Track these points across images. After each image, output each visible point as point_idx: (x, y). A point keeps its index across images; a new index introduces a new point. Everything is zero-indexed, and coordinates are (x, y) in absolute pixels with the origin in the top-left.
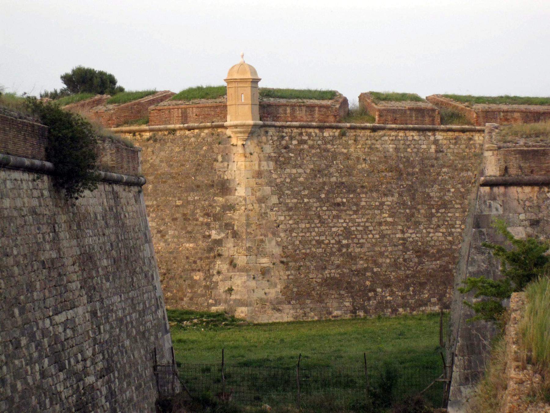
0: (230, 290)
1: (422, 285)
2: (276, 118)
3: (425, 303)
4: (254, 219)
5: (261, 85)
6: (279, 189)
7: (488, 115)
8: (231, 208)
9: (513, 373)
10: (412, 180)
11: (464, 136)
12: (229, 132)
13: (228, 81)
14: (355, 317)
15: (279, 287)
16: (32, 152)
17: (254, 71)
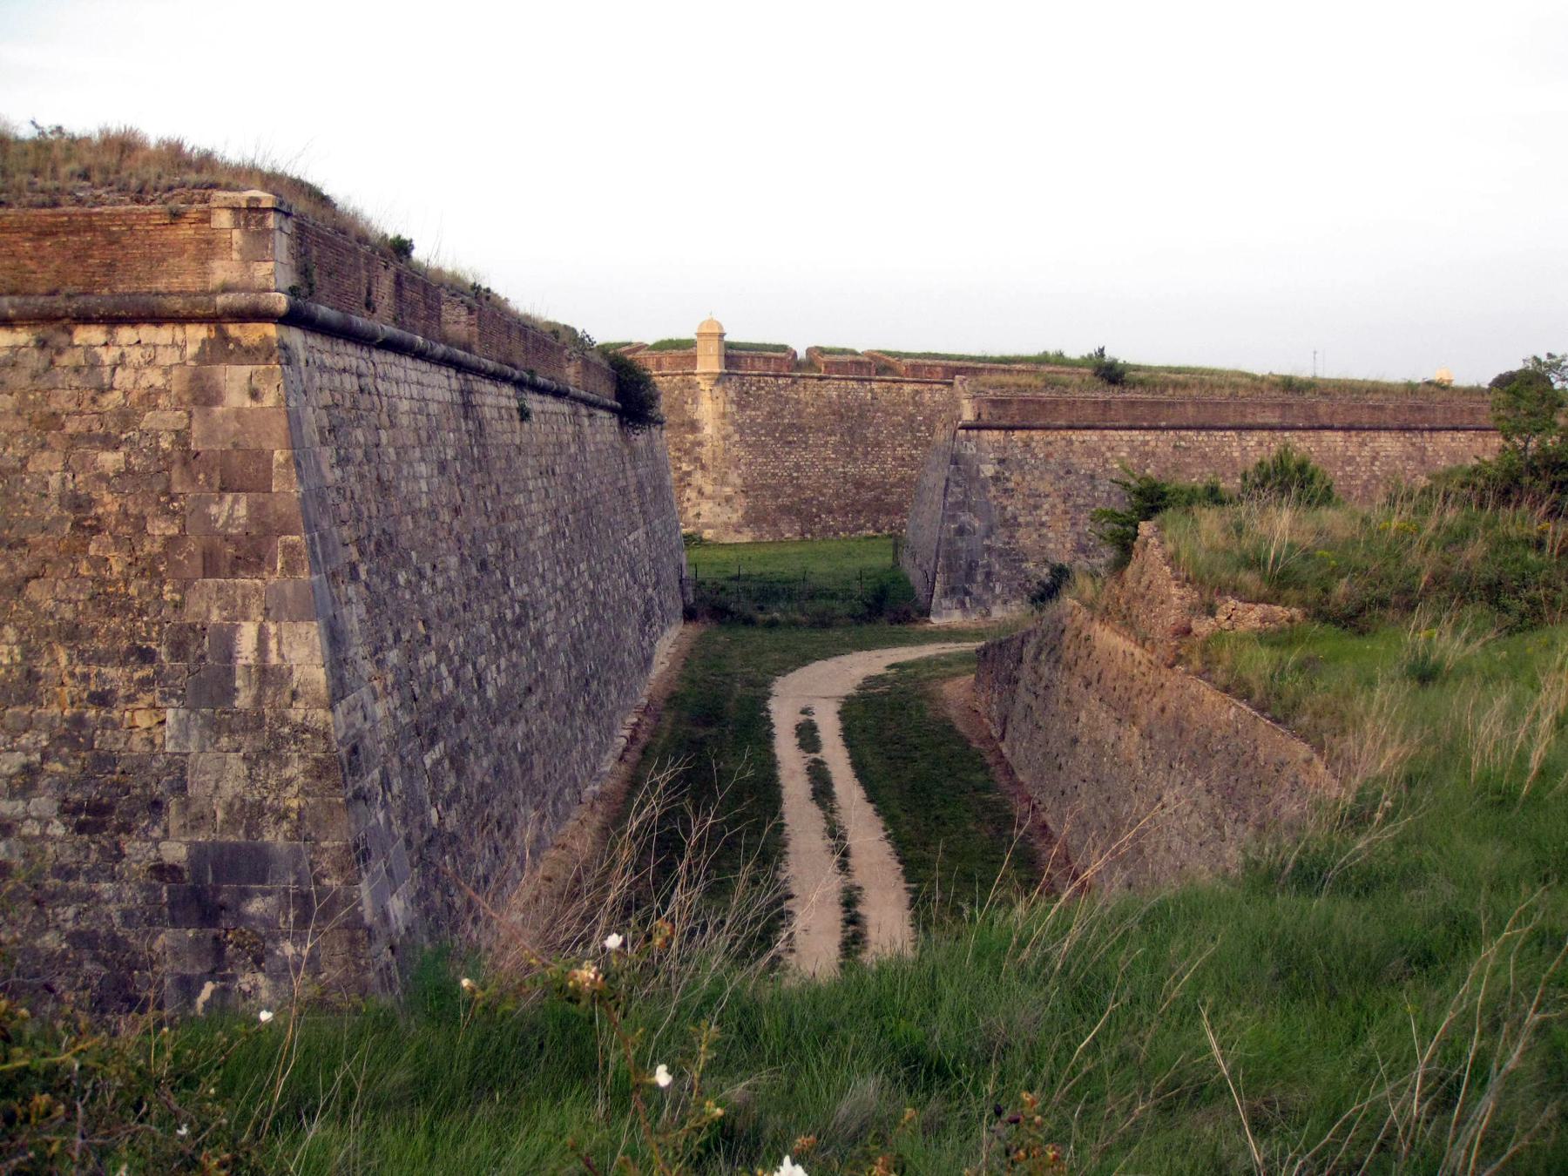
0: (698, 515)
1: (859, 512)
2: (738, 367)
3: (861, 528)
4: (719, 452)
5: (726, 338)
6: (740, 429)
7: (915, 368)
8: (700, 444)
9: (1174, 590)
10: (851, 423)
11: (895, 386)
12: (698, 379)
13: (699, 335)
14: (804, 540)
15: (740, 513)
16: (604, 391)
17: (721, 327)
